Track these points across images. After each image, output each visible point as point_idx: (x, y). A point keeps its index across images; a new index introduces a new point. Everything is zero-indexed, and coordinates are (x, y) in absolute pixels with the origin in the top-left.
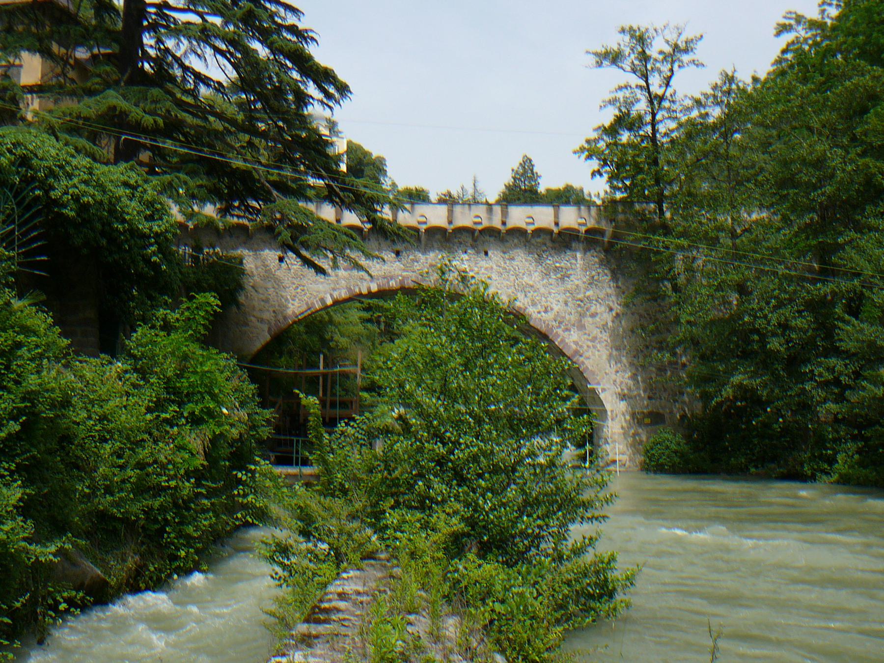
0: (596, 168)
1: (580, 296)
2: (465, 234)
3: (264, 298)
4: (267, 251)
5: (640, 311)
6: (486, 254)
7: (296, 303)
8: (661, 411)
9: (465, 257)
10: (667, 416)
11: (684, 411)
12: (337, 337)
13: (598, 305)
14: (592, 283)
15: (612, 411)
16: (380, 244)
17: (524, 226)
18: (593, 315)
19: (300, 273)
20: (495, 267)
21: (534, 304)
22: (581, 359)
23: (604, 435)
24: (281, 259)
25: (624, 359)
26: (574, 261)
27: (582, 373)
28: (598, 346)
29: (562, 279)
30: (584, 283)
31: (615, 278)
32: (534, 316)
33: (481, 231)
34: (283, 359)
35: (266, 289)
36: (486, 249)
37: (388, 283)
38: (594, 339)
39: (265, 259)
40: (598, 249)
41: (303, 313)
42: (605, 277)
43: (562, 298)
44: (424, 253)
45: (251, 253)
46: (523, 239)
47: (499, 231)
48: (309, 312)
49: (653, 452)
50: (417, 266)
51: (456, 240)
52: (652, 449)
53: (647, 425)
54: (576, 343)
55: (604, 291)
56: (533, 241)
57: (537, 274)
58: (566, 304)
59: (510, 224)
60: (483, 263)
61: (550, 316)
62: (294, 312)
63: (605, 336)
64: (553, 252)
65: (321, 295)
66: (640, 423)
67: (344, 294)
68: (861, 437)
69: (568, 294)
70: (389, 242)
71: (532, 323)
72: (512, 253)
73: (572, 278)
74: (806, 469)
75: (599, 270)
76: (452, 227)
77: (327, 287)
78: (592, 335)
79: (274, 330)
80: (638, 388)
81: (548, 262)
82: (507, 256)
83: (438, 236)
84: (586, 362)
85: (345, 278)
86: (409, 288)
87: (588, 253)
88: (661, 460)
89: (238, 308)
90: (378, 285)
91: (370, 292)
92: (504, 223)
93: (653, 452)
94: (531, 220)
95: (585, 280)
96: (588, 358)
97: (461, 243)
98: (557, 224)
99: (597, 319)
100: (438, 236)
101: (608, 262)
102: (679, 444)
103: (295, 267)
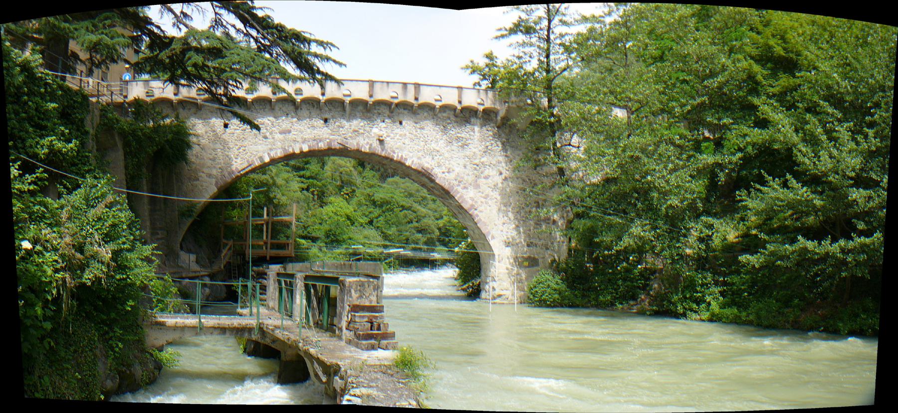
0: (477, 81)
1: (477, 161)
2: (383, 106)
3: (211, 157)
4: (214, 120)
5: (523, 176)
6: (401, 123)
7: (239, 161)
8: (536, 257)
9: (383, 125)
10: (540, 261)
11: (554, 257)
12: (279, 196)
13: (491, 169)
14: (486, 151)
15: (499, 255)
16: (310, 113)
17: (433, 102)
18: (486, 178)
19: (241, 137)
20: (408, 134)
21: (439, 166)
22: (476, 212)
23: (491, 274)
24: (226, 126)
25: (510, 214)
26: (472, 133)
27: (476, 224)
28: (490, 202)
29: (462, 147)
30: (480, 151)
31: (504, 149)
32: (440, 175)
33: (397, 105)
34: (235, 211)
35: (215, 150)
36: (401, 119)
37: (318, 144)
38: (486, 197)
39: (214, 126)
40: (492, 125)
41: (244, 169)
42: (497, 147)
43: (462, 162)
44: (348, 121)
45: (200, 121)
46: (431, 113)
47: (412, 106)
48: (250, 168)
49: (537, 289)
50: (342, 131)
51: (376, 111)
52: (535, 287)
53: (526, 267)
54: (472, 199)
55: (495, 159)
56: (440, 115)
57: (442, 142)
58: (465, 167)
59: (422, 100)
60: (398, 130)
61: (452, 176)
62: (237, 168)
63: (496, 195)
64: (455, 124)
65: (260, 154)
66: (520, 265)
67: (279, 153)
68: (724, 283)
69: (467, 159)
70: (318, 112)
71: (437, 181)
72: (423, 123)
73: (470, 146)
74: (679, 308)
75: (492, 142)
76: (372, 100)
77: (265, 148)
78: (485, 194)
79: (221, 183)
80: (520, 237)
81: (451, 132)
82: (418, 126)
83: (361, 108)
84: (480, 214)
85: (281, 141)
86: (335, 149)
87: (484, 128)
88: (544, 297)
89: (186, 163)
90: (309, 146)
91: (302, 152)
92: (416, 99)
93: (537, 289)
94: (439, 98)
95: (480, 148)
96: (481, 212)
97: (379, 114)
98: (460, 102)
99: (490, 181)
100: (361, 108)
101: (500, 136)
102: (557, 283)
103: (238, 131)
